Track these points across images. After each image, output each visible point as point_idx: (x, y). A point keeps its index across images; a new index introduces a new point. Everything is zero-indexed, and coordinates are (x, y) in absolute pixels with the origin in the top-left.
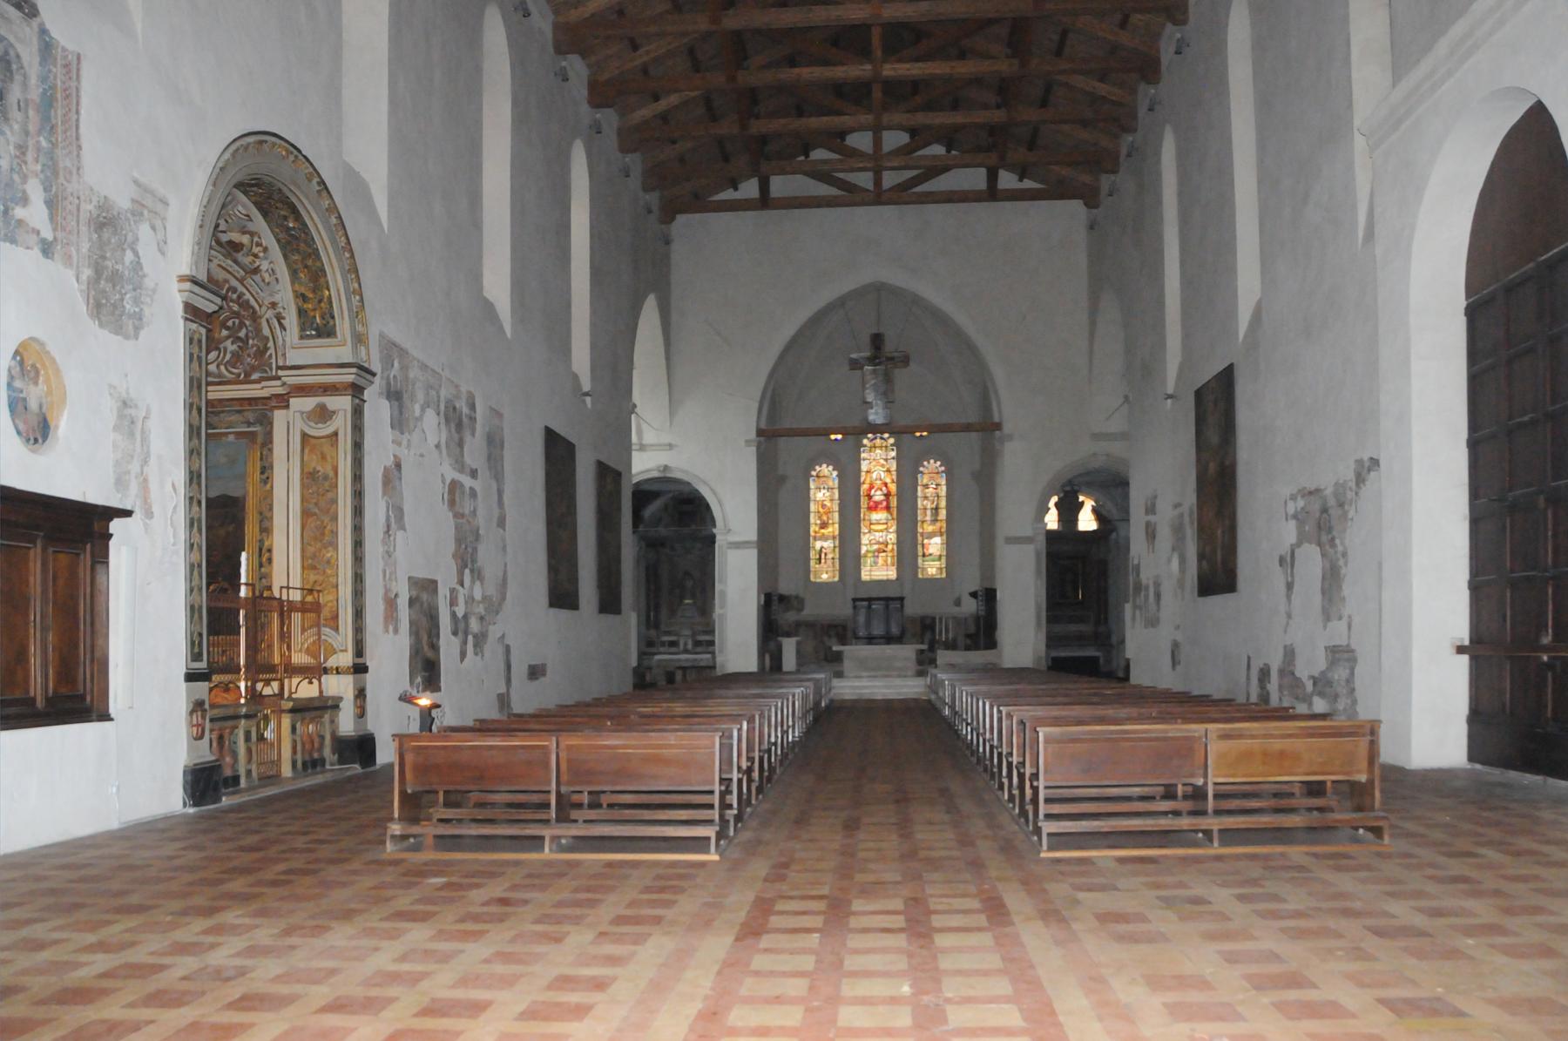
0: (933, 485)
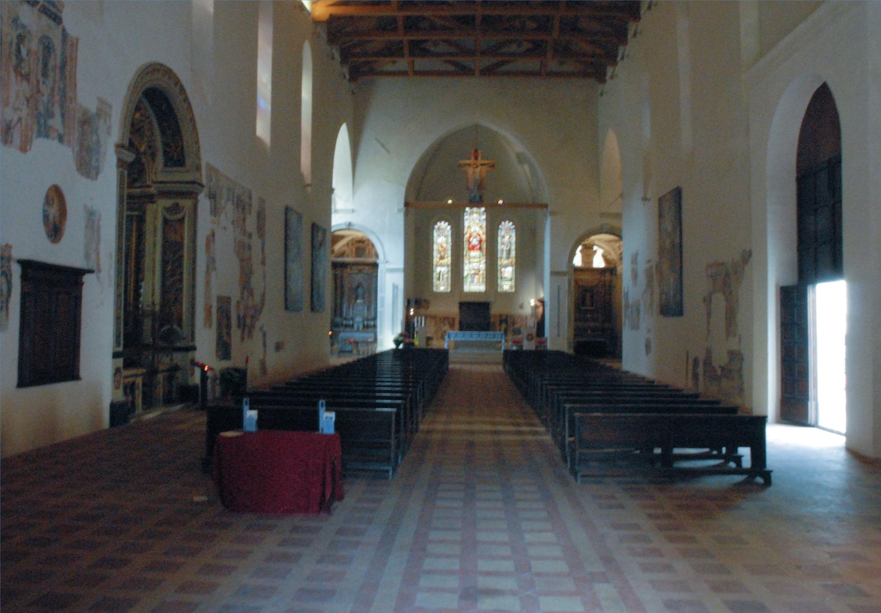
0: (507, 235)
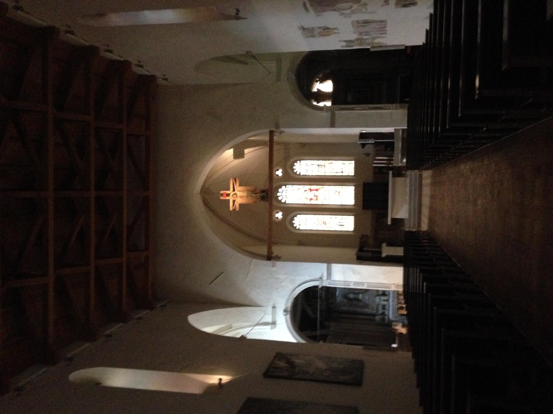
0: (305, 167)
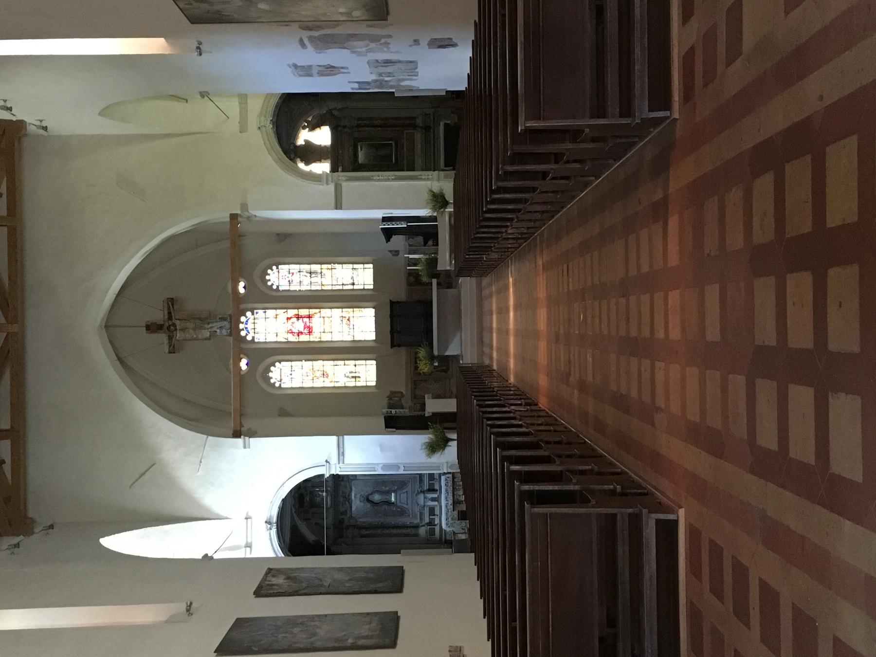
0: (285, 277)
